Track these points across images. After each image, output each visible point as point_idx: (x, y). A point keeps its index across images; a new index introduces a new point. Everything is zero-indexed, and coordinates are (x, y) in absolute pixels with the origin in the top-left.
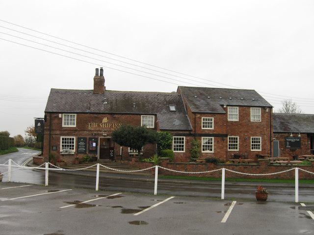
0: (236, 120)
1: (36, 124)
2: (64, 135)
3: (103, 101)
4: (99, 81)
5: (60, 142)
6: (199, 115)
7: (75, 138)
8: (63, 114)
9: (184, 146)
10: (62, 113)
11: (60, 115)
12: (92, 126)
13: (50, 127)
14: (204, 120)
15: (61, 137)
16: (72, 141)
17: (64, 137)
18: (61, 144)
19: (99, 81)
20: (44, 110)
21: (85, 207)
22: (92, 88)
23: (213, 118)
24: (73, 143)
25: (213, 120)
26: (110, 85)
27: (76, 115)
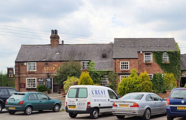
0: (152, 57)
1: (8, 71)
2: (28, 77)
3: (56, 52)
4: (55, 36)
5: (26, 82)
6: (118, 60)
7: (36, 78)
8: (27, 63)
9: (36, 84)
10: (26, 62)
11: (25, 64)
12: (46, 70)
13: (19, 72)
14: (122, 63)
15: (27, 79)
16: (34, 81)
17: (29, 78)
18: (27, 83)
19: (55, 36)
20: (14, 60)
21: (78, 94)
22: (50, 43)
23: (128, 62)
24: (35, 82)
25: (129, 63)
26: (63, 38)
27: (36, 63)
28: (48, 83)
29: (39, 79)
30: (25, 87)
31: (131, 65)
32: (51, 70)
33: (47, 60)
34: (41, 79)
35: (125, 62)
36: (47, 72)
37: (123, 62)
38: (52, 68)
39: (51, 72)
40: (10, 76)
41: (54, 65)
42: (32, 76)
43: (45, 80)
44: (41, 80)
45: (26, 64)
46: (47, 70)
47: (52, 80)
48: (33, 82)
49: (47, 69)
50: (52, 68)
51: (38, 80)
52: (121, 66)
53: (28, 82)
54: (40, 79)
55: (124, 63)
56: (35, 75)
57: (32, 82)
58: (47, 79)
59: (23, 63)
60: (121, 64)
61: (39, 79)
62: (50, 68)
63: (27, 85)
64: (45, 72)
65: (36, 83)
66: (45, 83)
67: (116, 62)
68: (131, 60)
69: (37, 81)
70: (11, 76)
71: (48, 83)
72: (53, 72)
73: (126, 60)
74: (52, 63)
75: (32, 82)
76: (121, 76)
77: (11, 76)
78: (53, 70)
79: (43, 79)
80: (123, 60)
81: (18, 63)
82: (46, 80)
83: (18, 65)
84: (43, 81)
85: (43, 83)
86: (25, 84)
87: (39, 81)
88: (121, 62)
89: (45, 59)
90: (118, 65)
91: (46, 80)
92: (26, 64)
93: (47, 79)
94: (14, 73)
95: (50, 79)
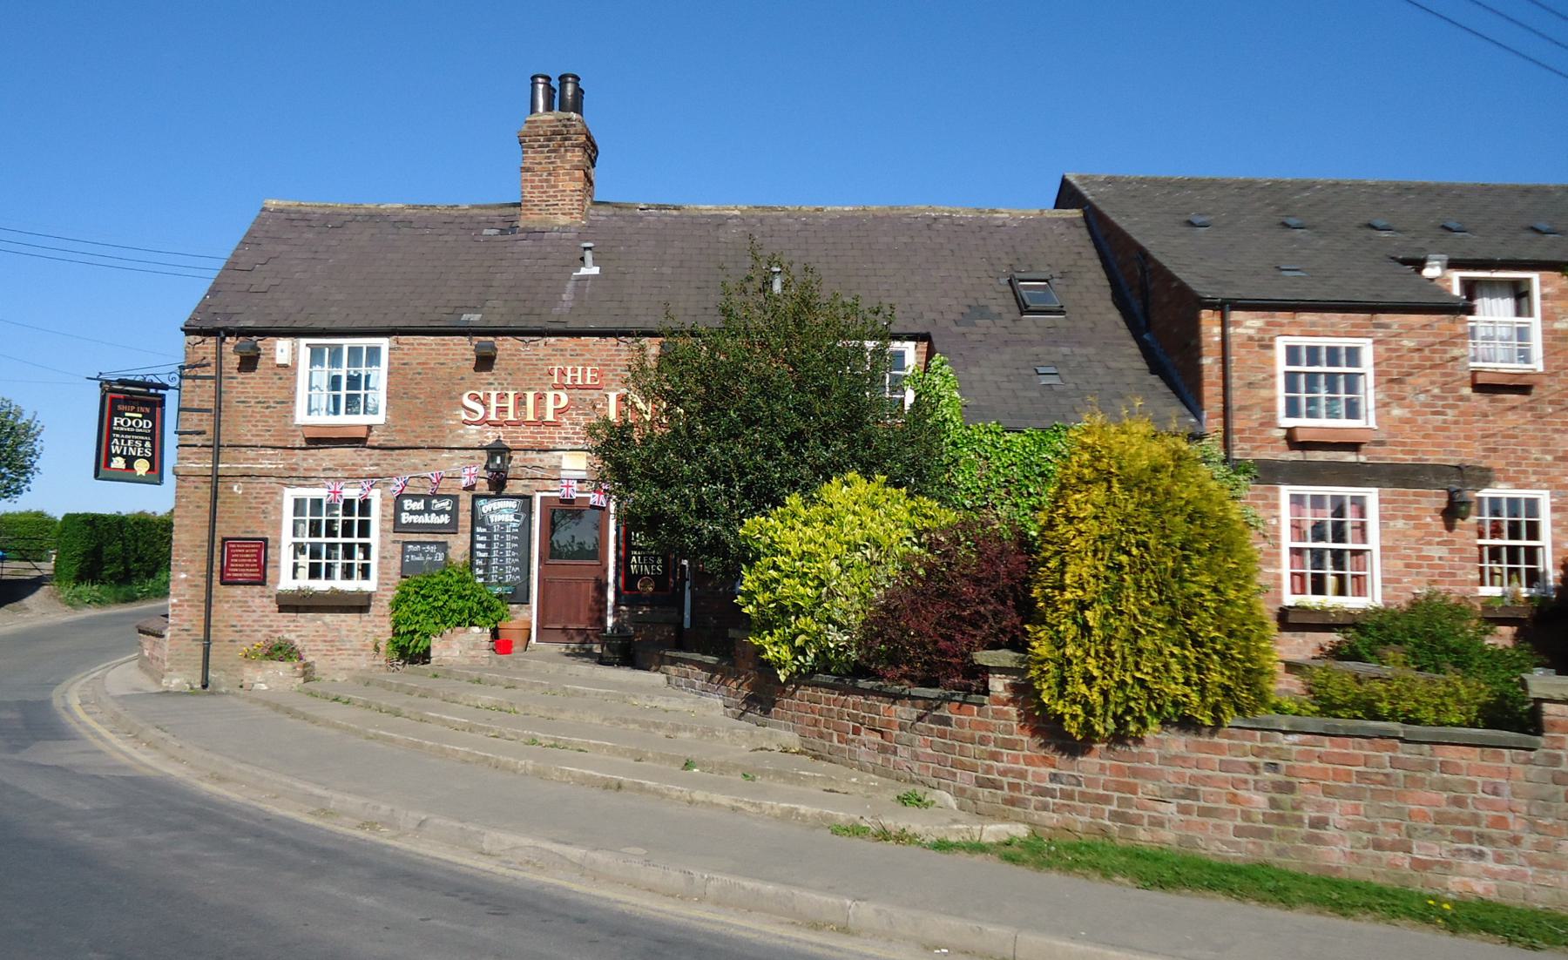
2: (305, 480)
5: (277, 525)
11: (282, 349)
13: (218, 424)
14: (1293, 354)
15: (289, 495)
17: (309, 493)
24: (364, 529)
27: (384, 343)
28: (489, 544)
29: (408, 504)
30: (262, 582)
31: (1391, 380)
32: (530, 417)
33: (496, 322)
34: (428, 499)
35: (1323, 342)
36: (490, 436)
37: (1304, 342)
38: (540, 398)
39: (524, 436)
40: (118, 463)
41: (563, 373)
42: (343, 466)
43: (465, 517)
44: (428, 509)
45: (295, 352)
46: (493, 417)
47: (530, 512)
48: (347, 531)
49: (493, 403)
50: (540, 398)
51: (399, 509)
52: (1281, 382)
53: (366, 548)
54: (420, 505)
55: (1313, 354)
56: (364, 460)
57: (339, 528)
58: (485, 507)
59: (263, 344)
60: (1281, 366)
61: (408, 504)
62: (520, 401)
63: (286, 557)
64: (473, 435)
65: (374, 539)
66: (459, 545)
67: (1234, 342)
68: (1395, 321)
69: (383, 519)
70: (130, 461)
71: (489, 544)
72: (544, 436)
73: (1336, 318)
74: (543, 346)
75: (339, 528)
76: (1285, 491)
77: (130, 461)
78: (550, 417)
79: (446, 504)
80: (1306, 317)
81: (211, 342)
82: (474, 509)
83: (211, 358)
84: (445, 519)
85: (443, 546)
86: (261, 549)
87: (405, 518)
88: (1281, 344)
89: (474, 309)
90: (883, 614)
91: (474, 509)
92: (295, 352)
93: (485, 507)
94: (687, 625)
95: (512, 504)
